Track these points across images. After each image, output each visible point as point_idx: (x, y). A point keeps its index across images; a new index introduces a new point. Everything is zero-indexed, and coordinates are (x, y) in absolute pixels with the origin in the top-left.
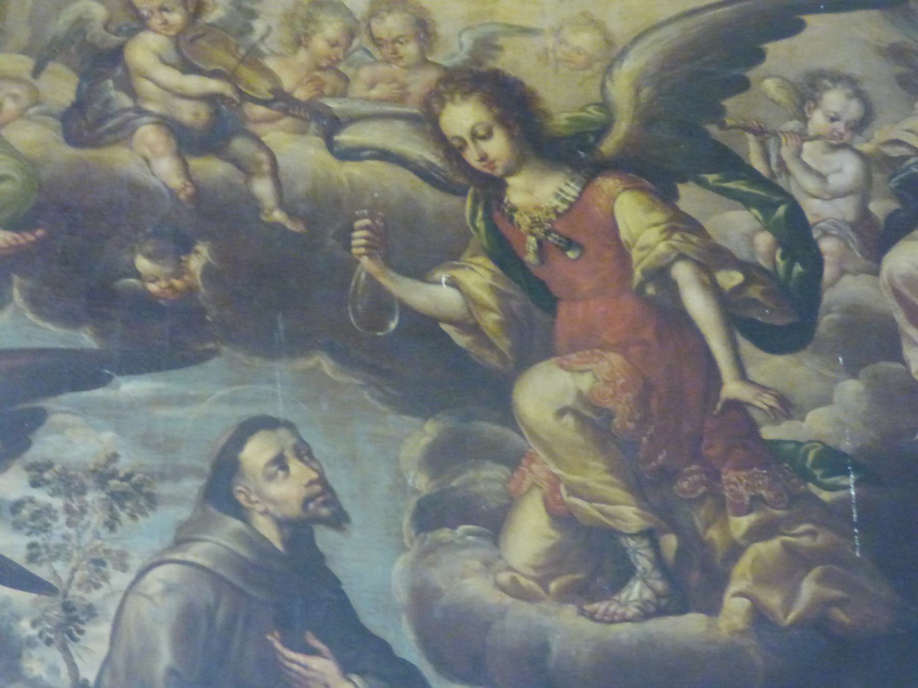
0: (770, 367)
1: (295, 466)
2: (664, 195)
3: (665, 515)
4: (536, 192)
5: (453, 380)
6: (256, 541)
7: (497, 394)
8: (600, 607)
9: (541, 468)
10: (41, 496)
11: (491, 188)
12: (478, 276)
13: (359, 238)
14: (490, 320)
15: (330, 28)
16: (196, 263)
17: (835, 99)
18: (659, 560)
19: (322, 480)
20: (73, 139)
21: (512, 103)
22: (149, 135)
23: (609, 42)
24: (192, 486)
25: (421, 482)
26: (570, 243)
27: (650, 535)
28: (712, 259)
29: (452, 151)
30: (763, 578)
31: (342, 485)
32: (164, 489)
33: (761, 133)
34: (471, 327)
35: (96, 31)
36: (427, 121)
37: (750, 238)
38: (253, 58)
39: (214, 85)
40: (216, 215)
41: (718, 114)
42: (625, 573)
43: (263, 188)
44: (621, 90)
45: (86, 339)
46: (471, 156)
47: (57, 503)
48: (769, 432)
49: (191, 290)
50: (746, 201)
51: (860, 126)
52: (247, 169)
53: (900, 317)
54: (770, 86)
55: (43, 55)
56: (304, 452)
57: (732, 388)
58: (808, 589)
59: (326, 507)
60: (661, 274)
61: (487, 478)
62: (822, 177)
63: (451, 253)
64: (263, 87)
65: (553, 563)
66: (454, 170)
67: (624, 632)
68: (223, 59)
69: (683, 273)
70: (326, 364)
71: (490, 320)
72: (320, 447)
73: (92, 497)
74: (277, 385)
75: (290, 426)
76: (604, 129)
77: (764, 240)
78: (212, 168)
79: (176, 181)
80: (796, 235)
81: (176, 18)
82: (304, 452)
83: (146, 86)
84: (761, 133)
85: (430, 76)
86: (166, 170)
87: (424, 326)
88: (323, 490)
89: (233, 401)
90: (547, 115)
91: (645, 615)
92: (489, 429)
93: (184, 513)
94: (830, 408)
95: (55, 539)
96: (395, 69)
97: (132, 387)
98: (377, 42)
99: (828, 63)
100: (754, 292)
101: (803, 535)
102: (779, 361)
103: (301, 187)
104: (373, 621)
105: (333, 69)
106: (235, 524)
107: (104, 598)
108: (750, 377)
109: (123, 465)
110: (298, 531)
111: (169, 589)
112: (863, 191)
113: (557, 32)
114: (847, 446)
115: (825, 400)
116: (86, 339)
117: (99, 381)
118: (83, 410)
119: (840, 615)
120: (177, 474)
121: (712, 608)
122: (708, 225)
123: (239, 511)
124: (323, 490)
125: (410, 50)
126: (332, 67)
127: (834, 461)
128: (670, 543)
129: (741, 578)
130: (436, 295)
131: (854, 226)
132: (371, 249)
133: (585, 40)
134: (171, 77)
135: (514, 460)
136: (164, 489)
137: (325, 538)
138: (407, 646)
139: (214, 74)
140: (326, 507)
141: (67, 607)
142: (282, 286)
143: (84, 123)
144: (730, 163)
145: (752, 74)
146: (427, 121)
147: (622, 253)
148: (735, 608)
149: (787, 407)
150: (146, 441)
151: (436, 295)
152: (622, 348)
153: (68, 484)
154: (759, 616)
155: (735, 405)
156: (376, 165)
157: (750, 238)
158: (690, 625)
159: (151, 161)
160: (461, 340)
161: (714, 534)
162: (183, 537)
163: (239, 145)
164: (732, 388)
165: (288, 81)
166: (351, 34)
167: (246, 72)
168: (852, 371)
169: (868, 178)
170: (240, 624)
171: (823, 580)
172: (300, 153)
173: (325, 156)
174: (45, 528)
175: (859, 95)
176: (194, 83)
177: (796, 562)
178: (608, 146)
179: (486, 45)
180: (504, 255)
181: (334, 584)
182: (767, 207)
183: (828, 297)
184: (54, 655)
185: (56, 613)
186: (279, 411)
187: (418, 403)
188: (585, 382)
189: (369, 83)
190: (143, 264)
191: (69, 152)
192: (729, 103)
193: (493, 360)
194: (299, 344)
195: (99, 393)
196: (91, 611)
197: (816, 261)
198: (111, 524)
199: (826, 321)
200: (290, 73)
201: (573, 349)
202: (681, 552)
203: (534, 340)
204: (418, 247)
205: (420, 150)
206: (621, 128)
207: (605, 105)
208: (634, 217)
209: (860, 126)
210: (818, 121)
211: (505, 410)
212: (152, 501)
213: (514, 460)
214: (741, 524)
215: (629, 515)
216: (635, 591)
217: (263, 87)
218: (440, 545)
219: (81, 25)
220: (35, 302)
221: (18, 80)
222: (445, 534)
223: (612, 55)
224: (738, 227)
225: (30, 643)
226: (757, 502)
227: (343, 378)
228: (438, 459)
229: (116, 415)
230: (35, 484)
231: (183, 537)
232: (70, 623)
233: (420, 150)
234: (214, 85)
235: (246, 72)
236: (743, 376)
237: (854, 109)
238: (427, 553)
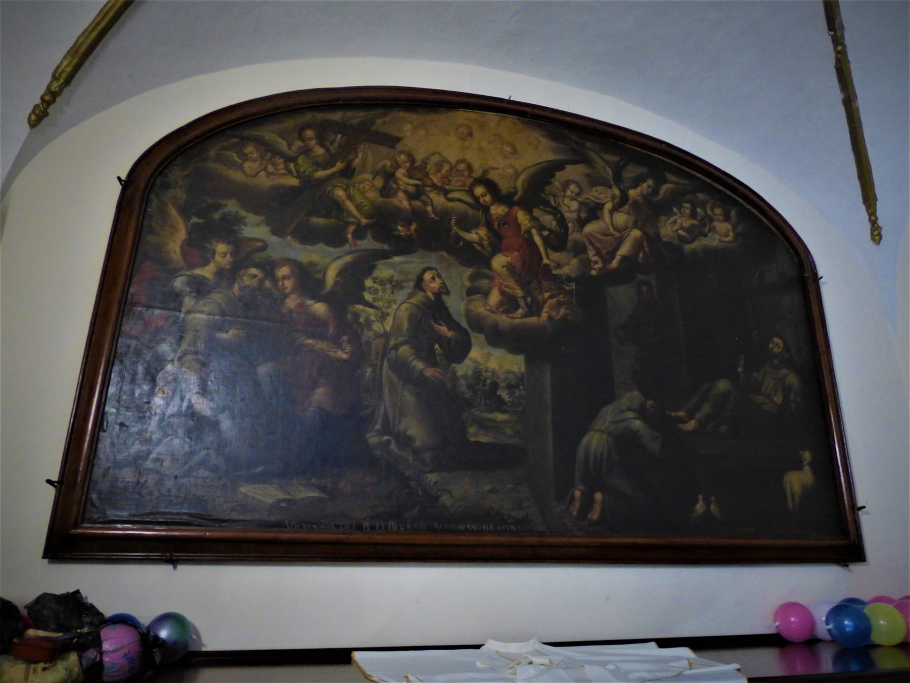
0: (556, 256)
1: (437, 279)
2: (529, 211)
3: (528, 293)
4: (498, 210)
5: (475, 258)
6: (427, 298)
7: (487, 262)
8: (511, 315)
9: (498, 280)
10: (376, 286)
11: (486, 209)
12: (483, 232)
13: (453, 222)
14: (486, 243)
15: (446, 167)
16: (413, 228)
17: (573, 187)
18: (526, 304)
19: (443, 283)
20: (383, 196)
21: (491, 187)
22: (401, 195)
23: (517, 172)
24: (412, 284)
25: (468, 284)
26: (505, 223)
27: (524, 298)
28: (541, 228)
29: (476, 199)
30: (553, 308)
31: (448, 284)
32: (405, 284)
33: (555, 196)
34: (481, 244)
35: (388, 168)
36: (470, 192)
37: (551, 222)
38: (427, 175)
39: (417, 182)
40: (417, 215)
41: (543, 191)
42: (517, 307)
43: (429, 209)
44: (519, 183)
45: (386, 247)
46: (481, 200)
47: (380, 288)
48: (554, 272)
49: (411, 235)
50: (549, 213)
51: (579, 194)
52: (425, 204)
53: (587, 243)
54: (557, 183)
55: (376, 174)
56: (439, 276)
57: (545, 261)
58: (562, 311)
59: (444, 290)
60: (528, 232)
61: (484, 283)
62: (569, 207)
63: (475, 225)
64: (429, 183)
65: (501, 304)
66: (477, 204)
67: (518, 321)
68: (419, 175)
69: (534, 231)
70: (445, 254)
71: (486, 243)
72: (443, 275)
73: (388, 286)
74: (432, 259)
75: (436, 269)
76: (515, 194)
77: (554, 223)
78: (417, 203)
79: (408, 207)
80: (562, 222)
81: (408, 165)
82: (439, 276)
83: (401, 182)
84: (555, 196)
85: (470, 180)
86: (405, 204)
87: (469, 244)
88: (444, 286)
89: (422, 263)
90: (500, 190)
91: (522, 317)
92: (485, 271)
93: (410, 290)
94: (569, 266)
95: (379, 296)
96: (463, 178)
97: (397, 259)
98: (458, 171)
99: (571, 177)
100: (552, 237)
101: (561, 298)
102: (557, 254)
103: (439, 208)
104: (456, 318)
105: (446, 178)
106: (422, 293)
107: (391, 311)
108: (549, 258)
109: (395, 278)
110: (438, 295)
111: (406, 309)
112: (579, 211)
113: (503, 169)
114: (573, 275)
115: (568, 264)
116: (386, 247)
117: (389, 257)
118: (384, 264)
119: (570, 318)
120: (408, 281)
121: (538, 315)
122: (540, 219)
123: (424, 291)
124: (444, 286)
125: (466, 173)
126: (447, 177)
127: (569, 279)
128: (529, 299)
129: (546, 308)
130: (472, 236)
131: (577, 220)
132: (456, 224)
133: (510, 171)
134: (406, 180)
135: (491, 278)
136: (405, 284)
137: (445, 298)
138: (464, 324)
139: (417, 179)
140: (444, 290)
141: (383, 313)
142: (434, 234)
143: (385, 192)
144: (547, 203)
145: (552, 180)
146: (470, 192)
147: (518, 226)
148: (544, 315)
149: (559, 266)
150: (401, 273)
151: (472, 236)
152: (518, 250)
153: (382, 283)
154: (550, 318)
155: (546, 265)
156: (457, 202)
157: (551, 222)
158: (533, 320)
159: (401, 201)
160: (478, 248)
161: (540, 297)
162: (410, 296)
163: (424, 197)
164: (545, 261)
165: (435, 181)
166: (451, 169)
167: (425, 179)
168: (575, 257)
169: (580, 207)
170: (83, 503)
171: (566, 309)
172: (438, 199)
173: (445, 200)
174: (377, 294)
175: (579, 186)
176: (412, 182)
177: (559, 304)
178: (516, 198)
179: (485, 172)
180: (489, 225)
181: (446, 309)
182: (555, 215)
183: (570, 238)
184: (379, 324)
185: (380, 314)
186: (433, 265)
187: (467, 263)
188: (509, 259)
189: (456, 182)
190: (400, 228)
191: (382, 199)
192: (546, 188)
193: (485, 253)
194: (437, 249)
195: (389, 260)
196: (388, 314)
197: (567, 228)
198: (393, 293)
199: (569, 244)
200: (436, 179)
201: (507, 250)
202: (532, 301)
203: (496, 249)
204: (468, 224)
205: (469, 200)
206: (520, 193)
207: (515, 188)
208: (522, 217)
209: (579, 194)
210: (568, 193)
211: (489, 267)
212: (402, 288)
213: (491, 278)
214: (547, 295)
215: (519, 292)
216: (520, 311)
217: (429, 183)
218: (472, 299)
219: (384, 166)
220: (374, 237)
221: (368, 181)
222: (473, 297)
223: (517, 175)
224: (548, 220)
225: (374, 321)
226: (551, 289)
227: (450, 257)
228: (473, 278)
229: (393, 266)
230: (374, 282)
231: (410, 296)
232: (383, 317)
233: (469, 200)
234: (417, 182)
235: (425, 179)
236: (548, 258)
237: (577, 190)
238: (470, 301)
